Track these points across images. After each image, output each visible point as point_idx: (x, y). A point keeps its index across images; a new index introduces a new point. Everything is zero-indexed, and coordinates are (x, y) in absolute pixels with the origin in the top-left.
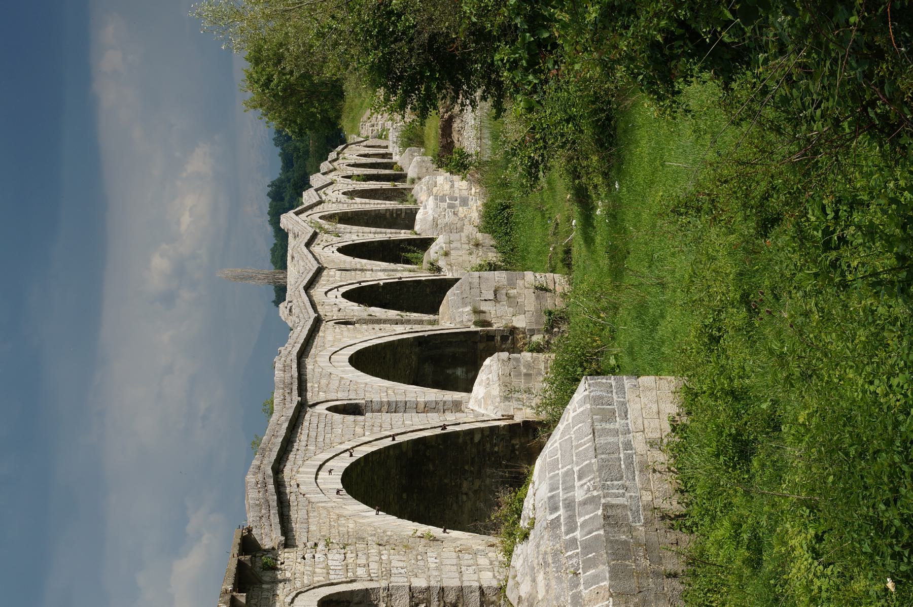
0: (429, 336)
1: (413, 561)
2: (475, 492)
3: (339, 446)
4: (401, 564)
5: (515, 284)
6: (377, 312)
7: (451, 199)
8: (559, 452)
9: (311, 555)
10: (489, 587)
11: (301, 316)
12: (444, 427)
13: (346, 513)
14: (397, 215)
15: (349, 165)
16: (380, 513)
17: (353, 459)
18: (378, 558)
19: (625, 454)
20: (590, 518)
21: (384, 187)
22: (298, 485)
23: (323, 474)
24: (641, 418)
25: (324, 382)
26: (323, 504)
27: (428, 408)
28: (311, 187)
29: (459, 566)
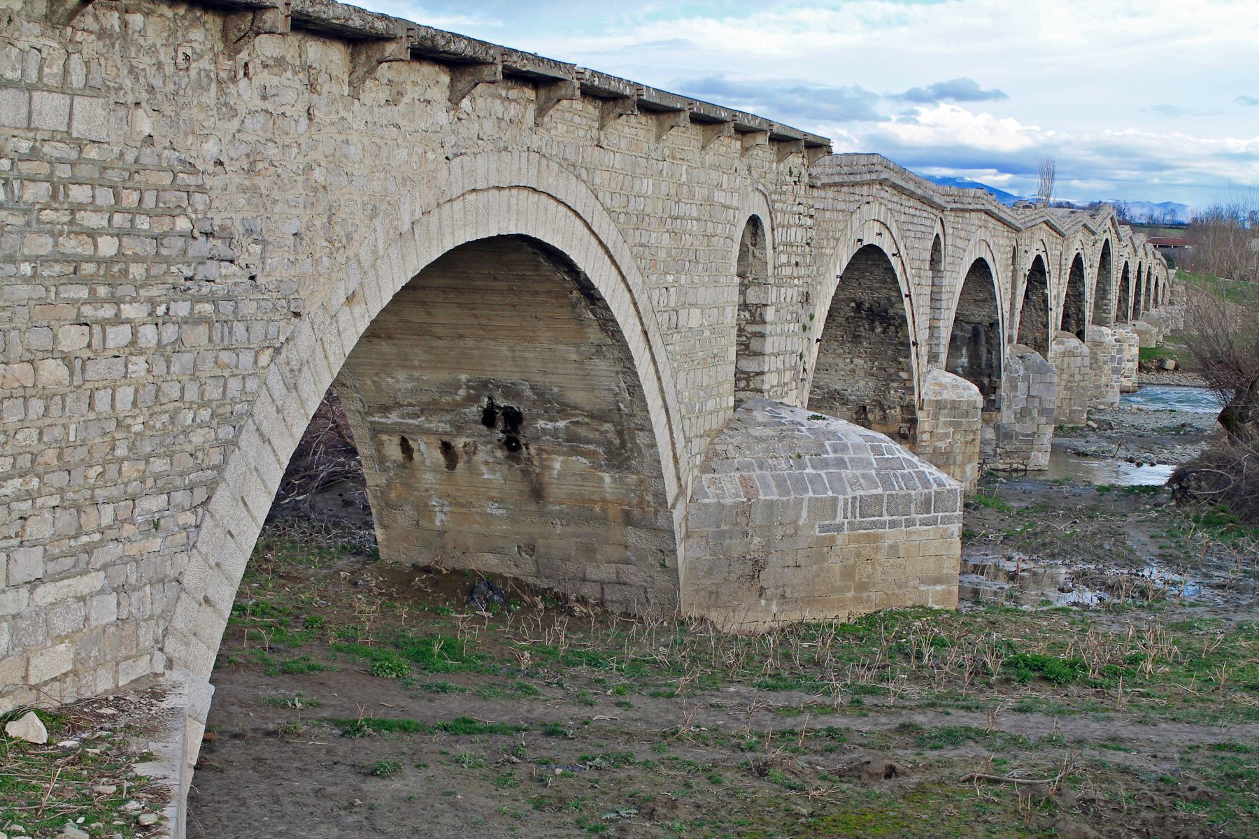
2: (853, 371)
4: (788, 300)
6: (1022, 288)
17: (890, 256)
23: (877, 227)
25: (962, 233)
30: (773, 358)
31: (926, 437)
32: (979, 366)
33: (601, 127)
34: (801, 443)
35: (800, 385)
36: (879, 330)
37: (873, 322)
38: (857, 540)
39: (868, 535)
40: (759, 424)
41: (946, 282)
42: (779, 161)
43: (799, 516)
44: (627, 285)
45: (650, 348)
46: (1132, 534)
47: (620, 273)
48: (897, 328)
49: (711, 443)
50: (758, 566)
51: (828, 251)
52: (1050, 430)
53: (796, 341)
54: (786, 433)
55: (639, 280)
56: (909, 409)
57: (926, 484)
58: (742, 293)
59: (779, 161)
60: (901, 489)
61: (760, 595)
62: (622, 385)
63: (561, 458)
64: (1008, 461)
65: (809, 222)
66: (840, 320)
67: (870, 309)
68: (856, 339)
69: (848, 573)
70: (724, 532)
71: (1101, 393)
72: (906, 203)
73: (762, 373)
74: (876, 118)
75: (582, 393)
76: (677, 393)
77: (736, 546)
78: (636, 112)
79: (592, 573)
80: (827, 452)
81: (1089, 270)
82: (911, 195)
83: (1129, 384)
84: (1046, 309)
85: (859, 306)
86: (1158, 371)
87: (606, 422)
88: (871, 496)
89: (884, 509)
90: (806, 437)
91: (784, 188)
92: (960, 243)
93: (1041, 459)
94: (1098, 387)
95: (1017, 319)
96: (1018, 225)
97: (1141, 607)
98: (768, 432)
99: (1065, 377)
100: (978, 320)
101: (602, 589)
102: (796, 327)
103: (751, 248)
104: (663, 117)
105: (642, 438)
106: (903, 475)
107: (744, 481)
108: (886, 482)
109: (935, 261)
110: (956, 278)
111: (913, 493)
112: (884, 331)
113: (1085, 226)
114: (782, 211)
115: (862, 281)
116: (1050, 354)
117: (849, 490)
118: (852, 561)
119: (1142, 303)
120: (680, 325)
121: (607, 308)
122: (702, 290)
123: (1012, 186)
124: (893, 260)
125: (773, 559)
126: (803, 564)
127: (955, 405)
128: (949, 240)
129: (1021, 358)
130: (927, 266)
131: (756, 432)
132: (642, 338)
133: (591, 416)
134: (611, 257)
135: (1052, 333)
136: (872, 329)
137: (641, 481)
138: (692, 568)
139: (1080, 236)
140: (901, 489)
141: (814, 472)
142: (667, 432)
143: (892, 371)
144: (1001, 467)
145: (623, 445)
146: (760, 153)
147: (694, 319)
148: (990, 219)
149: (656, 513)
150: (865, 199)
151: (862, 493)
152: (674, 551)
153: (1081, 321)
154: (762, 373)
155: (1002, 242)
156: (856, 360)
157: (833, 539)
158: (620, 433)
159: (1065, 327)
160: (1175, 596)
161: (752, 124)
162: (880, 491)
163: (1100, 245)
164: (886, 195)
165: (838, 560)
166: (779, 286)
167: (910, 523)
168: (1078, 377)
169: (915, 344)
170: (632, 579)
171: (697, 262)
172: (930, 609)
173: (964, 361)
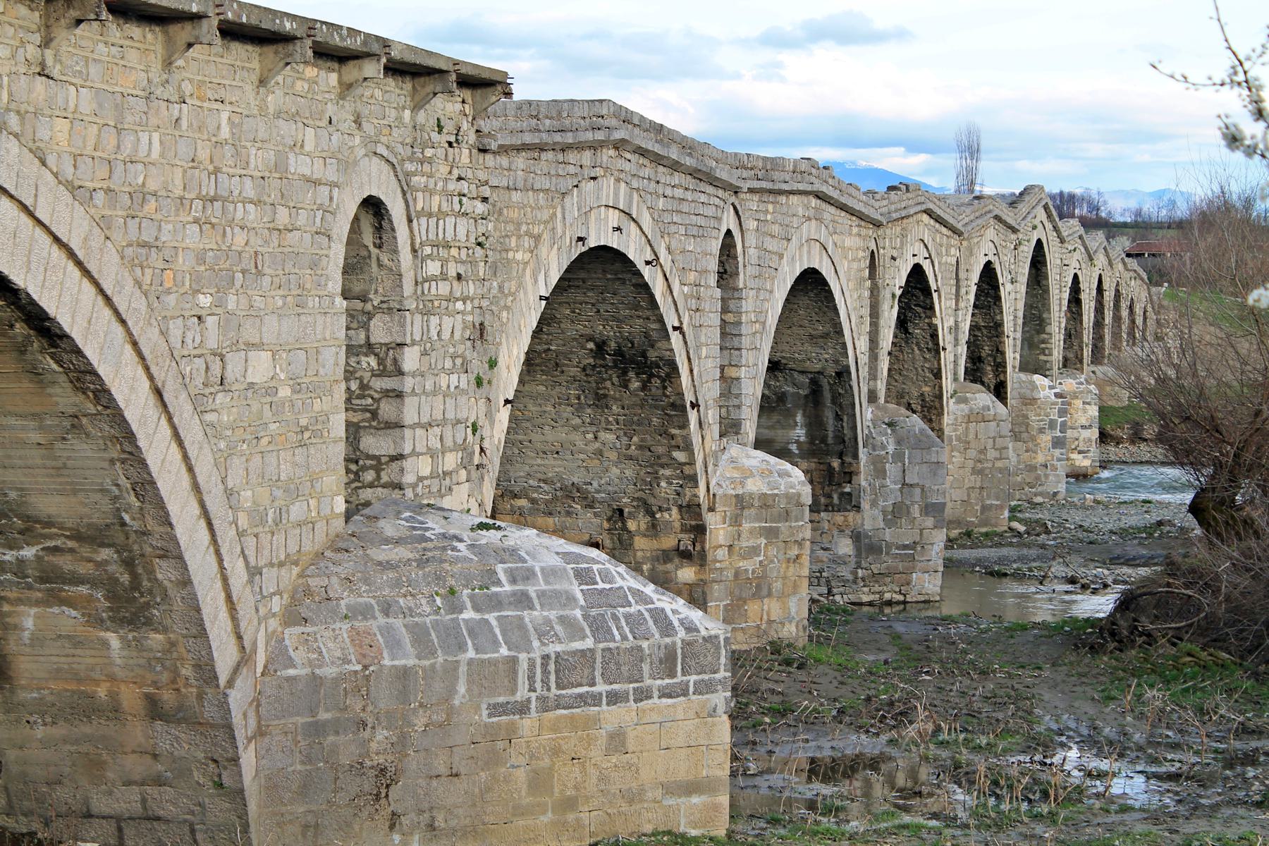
0: (851, 387)
1: (451, 350)
2: (599, 453)
3: (663, 245)
4: (446, 335)
5: (927, 514)
6: (890, 314)
7: (1064, 424)
8: (608, 586)
9: (466, 191)
10: (402, 470)
11: (885, 202)
12: (694, 405)
13: (543, 250)
14: (1044, 349)
15: (1118, 285)
16: (544, 303)
17: (640, 265)
18: (458, 295)
19: (601, 694)
20: (495, 635)
21: (1085, 333)
22: (594, 178)
23: (614, 218)
24: (660, 720)
25: (776, 229)
26: (559, 215)
27: (729, 384)
28: (1086, 233)
29: (443, 423)
30: (419, 432)
31: (722, 553)
32: (824, 440)
33: (46, 43)
34: (457, 568)
35: (475, 475)
36: (635, 385)
37: (625, 372)
38: (555, 728)
39: (572, 717)
40: (387, 541)
41: (748, 305)
42: (416, 108)
43: (452, 691)
44: (116, 312)
45: (170, 419)
46: (1046, 697)
47: (101, 291)
48: (663, 381)
49: (301, 576)
50: (385, 777)
51: (519, 256)
52: (939, 538)
53: (463, 408)
54: (431, 554)
55: (141, 304)
56: (691, 509)
57: (666, 627)
59: (416, 108)
60: (624, 638)
61: (392, 827)
62: (123, 481)
63: (33, 611)
65: (480, 208)
66: (574, 371)
67: (619, 352)
68: (600, 400)
69: (539, 782)
70: (325, 724)
71: (1038, 478)
72: (668, 180)
73: (400, 457)
75: (58, 499)
76: (229, 493)
77: (346, 747)
78: (105, 14)
79: (100, 804)
80: (498, 583)
81: (1009, 287)
82: (675, 166)
83: (1087, 463)
84: (936, 350)
85: (601, 347)
86: (1133, 442)
87: (103, 545)
88: (574, 653)
89: (598, 674)
90: (465, 559)
91: (429, 152)
92: (771, 245)
93: (928, 583)
94: (1032, 468)
97: (1038, 817)
98: (403, 553)
100: (818, 367)
101: (120, 830)
102: (464, 381)
103: (374, 251)
104: (174, 29)
105: (165, 572)
106: (628, 617)
107: (356, 635)
108: (599, 628)
109: (726, 274)
110: (766, 302)
111: (645, 644)
113: (997, 218)
114: (425, 189)
115: (602, 308)
116: (947, 419)
117: (536, 644)
118: (546, 762)
119: (1107, 338)
120: (229, 376)
121: (78, 352)
122: (271, 322)
123: (929, 171)
124: (646, 272)
125: (413, 762)
126: (463, 771)
127: (766, 502)
128: (751, 240)
129: (890, 425)
130: (713, 280)
131: (382, 553)
132: (152, 400)
133: (78, 536)
134: (79, 264)
135: (948, 384)
136: (625, 385)
137: (173, 644)
138: (272, 787)
139: (990, 233)
140: (624, 638)
141: (477, 616)
142: (212, 559)
143: (660, 450)
144: (865, 599)
145: (135, 584)
146: (378, 93)
147: (260, 367)
148: (824, 206)
149: (200, 697)
150: (587, 172)
151: (559, 648)
152: (235, 760)
153: (1000, 367)
154: (400, 457)
155: (849, 242)
156: (602, 435)
157: (512, 731)
158: (129, 564)
159: (974, 374)
160: (1098, 795)
161: (348, 43)
162: (589, 643)
163: (1028, 250)
164: (627, 167)
165: (522, 761)
166: (427, 313)
167: (643, 695)
168: (992, 454)
169: (694, 405)
170: (167, 810)
171: (260, 274)
172: (683, 836)
173: (800, 433)
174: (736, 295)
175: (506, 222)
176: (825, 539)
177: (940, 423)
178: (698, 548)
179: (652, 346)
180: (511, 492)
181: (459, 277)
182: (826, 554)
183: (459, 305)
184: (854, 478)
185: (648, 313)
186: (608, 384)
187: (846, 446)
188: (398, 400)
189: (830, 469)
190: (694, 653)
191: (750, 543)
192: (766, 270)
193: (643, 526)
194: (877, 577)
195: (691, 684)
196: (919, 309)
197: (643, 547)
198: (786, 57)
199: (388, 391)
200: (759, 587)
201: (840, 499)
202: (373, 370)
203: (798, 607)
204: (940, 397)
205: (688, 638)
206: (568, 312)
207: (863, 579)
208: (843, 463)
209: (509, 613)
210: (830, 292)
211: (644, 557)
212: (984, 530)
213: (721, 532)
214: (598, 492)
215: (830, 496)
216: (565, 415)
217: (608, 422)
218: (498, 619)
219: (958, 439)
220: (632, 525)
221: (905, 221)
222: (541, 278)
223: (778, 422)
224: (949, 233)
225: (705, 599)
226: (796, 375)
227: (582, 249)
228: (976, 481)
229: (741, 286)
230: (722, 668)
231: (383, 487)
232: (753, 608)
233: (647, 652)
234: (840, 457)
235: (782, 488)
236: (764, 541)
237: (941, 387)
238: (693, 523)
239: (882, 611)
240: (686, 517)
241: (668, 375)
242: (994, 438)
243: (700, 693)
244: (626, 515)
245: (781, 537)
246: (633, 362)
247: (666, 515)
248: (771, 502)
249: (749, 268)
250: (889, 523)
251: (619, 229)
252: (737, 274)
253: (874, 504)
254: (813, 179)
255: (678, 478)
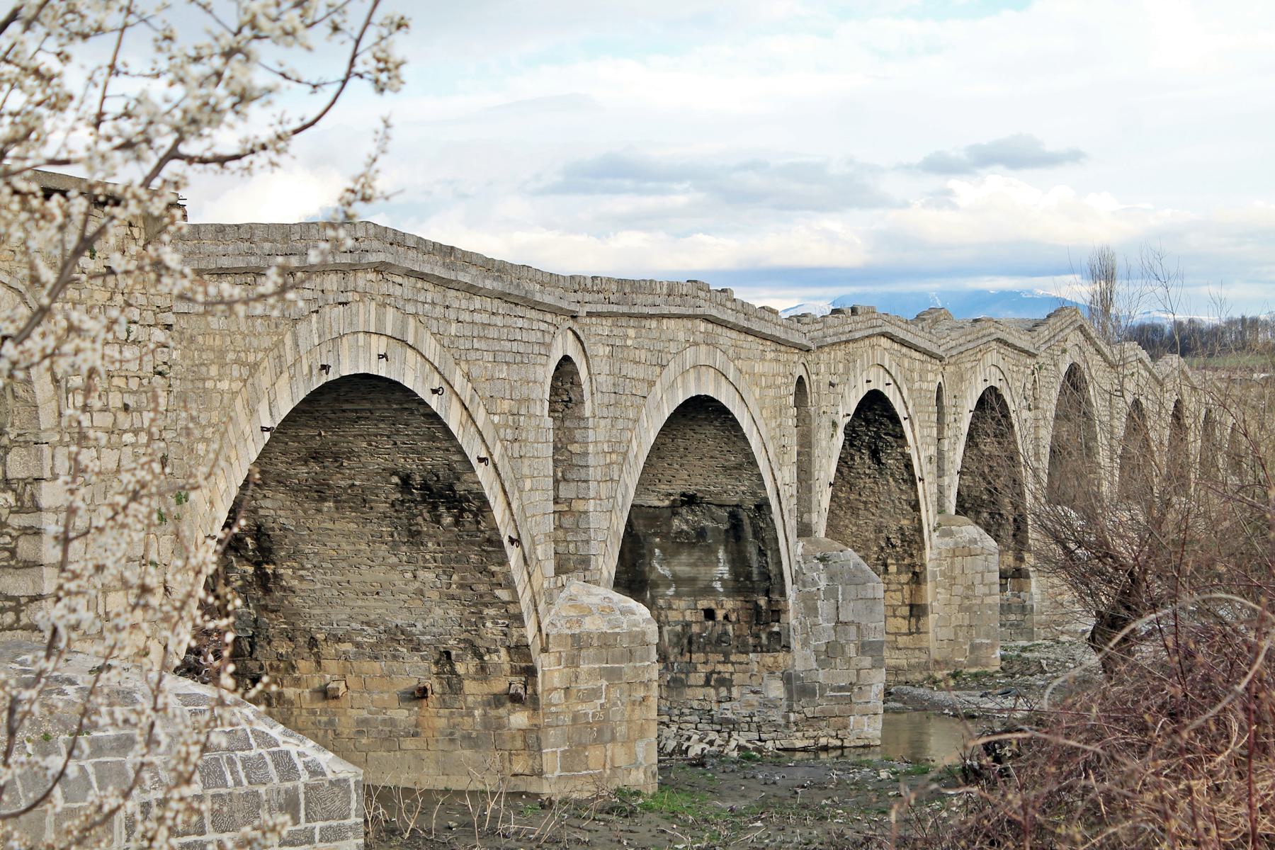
0: (772, 521)
2: (421, 593)
3: (458, 372)
5: (863, 653)
9: (137, 318)
16: (267, 435)
17: (424, 394)
18: (127, 426)
31: (557, 697)
32: (748, 577)
36: (447, 520)
48: (475, 515)
51: (224, 385)
56: (520, 650)
58: (556, 489)
60: (238, 783)
64: (811, 733)
66: (383, 507)
67: (425, 486)
68: (414, 537)
74: (883, 202)
84: (912, 482)
95: (824, 498)
96: (804, 342)
99: (958, 589)
100: (736, 500)
111: (262, 790)
112: (457, 523)
113: (999, 340)
115: (399, 440)
116: (928, 554)
124: (434, 402)
127: (606, 641)
128: (601, 366)
129: (822, 559)
135: (928, 516)
136: (437, 520)
139: (992, 357)
140: (238, 783)
143: (482, 588)
144: (799, 744)
148: (719, 330)
173: (723, 570)
174: (582, 424)
175: (201, 350)
176: (755, 681)
177: (922, 558)
178: (530, 691)
179: (458, 479)
180: (335, 636)
181: (126, 408)
182: (756, 697)
183: (129, 438)
184: (782, 616)
185: (447, 444)
186: (420, 520)
187: (772, 583)
188: (37, 538)
189: (757, 607)
190: (322, 797)
191: (590, 685)
192: (624, 397)
193: (472, 670)
194: (811, 721)
195: (317, 831)
196: (890, 439)
197: (473, 691)
198: (954, 183)
199: (26, 528)
200: (602, 732)
201: (768, 638)
202: (10, 507)
203: (647, 753)
204: (920, 530)
205: (312, 782)
206: (364, 445)
207: (796, 724)
208: (770, 601)
209: (109, 759)
210: (734, 420)
211: (475, 702)
212: (973, 670)
213: (556, 674)
214: (423, 634)
215: (757, 636)
216: (381, 553)
217: (426, 561)
218: (95, 765)
219: (943, 574)
220: (460, 668)
221: (851, 345)
222: (263, 408)
223: (700, 558)
224: (925, 358)
225: (539, 745)
226: (713, 508)
227: (318, 381)
228: (965, 618)
229: (588, 413)
230: (353, 813)
231: (23, 628)
232: (594, 754)
233: (265, 798)
234: (767, 595)
235: (625, 626)
236: (605, 683)
237: (920, 520)
238: (523, 665)
239: (817, 757)
240: (515, 658)
241: (479, 509)
242: (982, 574)
243: (327, 841)
244: (453, 658)
245: (624, 678)
246: (441, 497)
247: (495, 657)
248: (612, 641)
249: (598, 396)
250: (822, 664)
251: (385, 356)
252: (582, 402)
253: (805, 643)
254: (702, 302)
255: (503, 617)
